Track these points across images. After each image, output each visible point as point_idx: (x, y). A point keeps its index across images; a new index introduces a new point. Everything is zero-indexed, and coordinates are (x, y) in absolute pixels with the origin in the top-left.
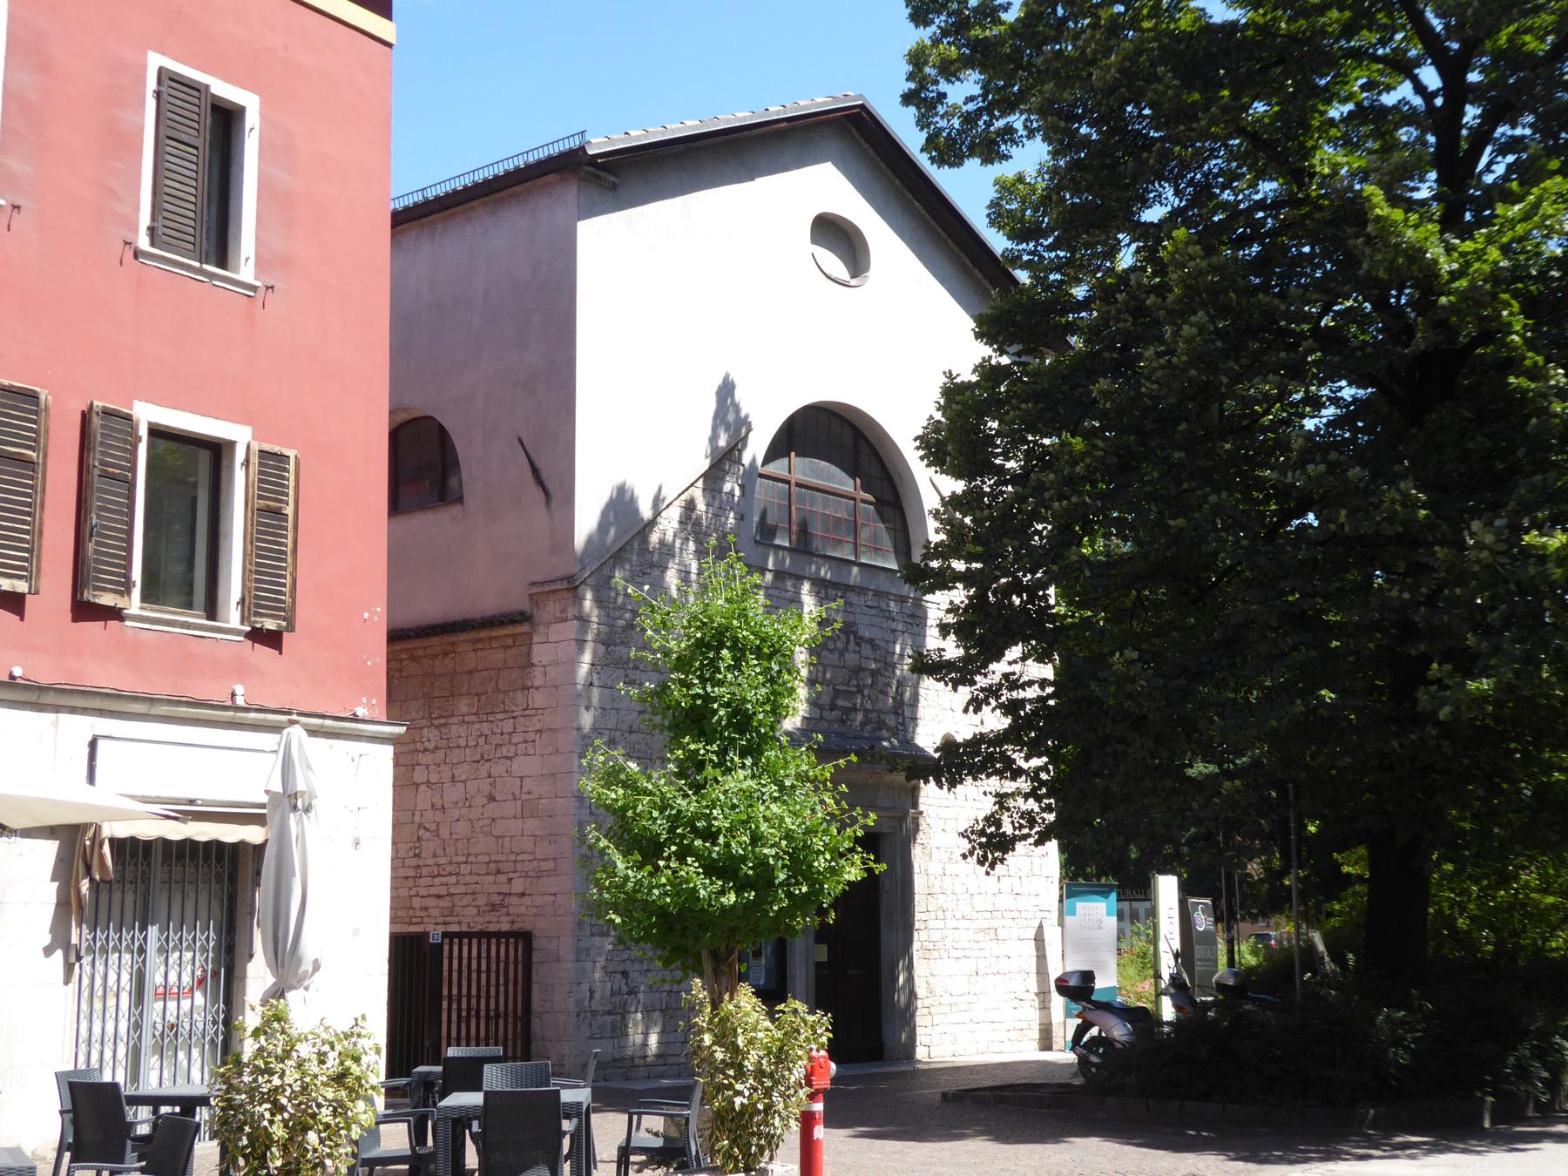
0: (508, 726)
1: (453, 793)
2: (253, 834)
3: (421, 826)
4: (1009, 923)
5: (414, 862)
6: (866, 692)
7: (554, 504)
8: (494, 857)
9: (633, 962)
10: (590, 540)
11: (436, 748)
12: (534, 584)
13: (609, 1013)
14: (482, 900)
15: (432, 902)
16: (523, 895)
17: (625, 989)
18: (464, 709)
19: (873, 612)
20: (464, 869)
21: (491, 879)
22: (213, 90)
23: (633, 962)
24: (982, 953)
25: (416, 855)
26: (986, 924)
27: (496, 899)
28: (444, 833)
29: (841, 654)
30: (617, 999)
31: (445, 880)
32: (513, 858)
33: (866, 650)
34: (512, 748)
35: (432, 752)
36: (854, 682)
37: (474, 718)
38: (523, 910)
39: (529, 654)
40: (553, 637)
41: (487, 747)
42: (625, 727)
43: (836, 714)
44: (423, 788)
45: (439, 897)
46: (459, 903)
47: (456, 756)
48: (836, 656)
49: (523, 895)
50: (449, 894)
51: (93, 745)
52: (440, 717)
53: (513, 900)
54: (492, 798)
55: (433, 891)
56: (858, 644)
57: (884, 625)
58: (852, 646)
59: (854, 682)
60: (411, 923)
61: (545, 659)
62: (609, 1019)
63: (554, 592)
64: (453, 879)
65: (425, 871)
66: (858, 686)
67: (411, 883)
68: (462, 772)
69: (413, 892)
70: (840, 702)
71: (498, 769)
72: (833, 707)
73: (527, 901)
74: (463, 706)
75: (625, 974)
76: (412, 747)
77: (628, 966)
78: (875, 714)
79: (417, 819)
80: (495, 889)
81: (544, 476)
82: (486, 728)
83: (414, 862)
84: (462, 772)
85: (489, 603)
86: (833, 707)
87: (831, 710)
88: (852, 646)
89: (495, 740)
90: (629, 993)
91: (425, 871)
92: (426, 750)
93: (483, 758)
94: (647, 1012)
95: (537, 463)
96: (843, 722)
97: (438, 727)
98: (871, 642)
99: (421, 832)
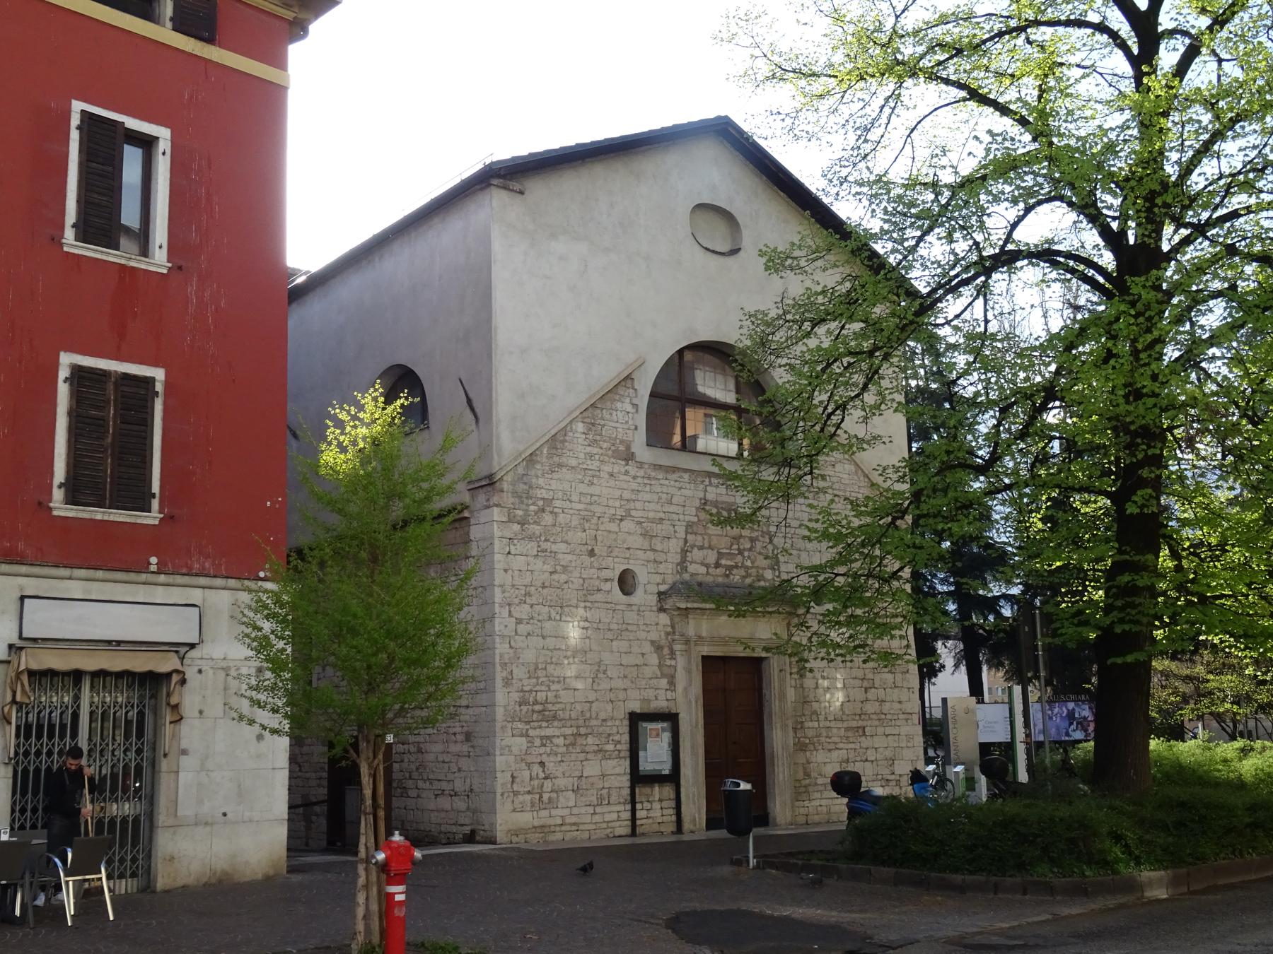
2: (165, 664)
6: (746, 554)
7: (481, 424)
13: (529, 792)
16: (468, 707)
22: (127, 125)
24: (852, 746)
26: (854, 724)
36: (735, 547)
39: (468, 534)
42: (539, 584)
43: (720, 571)
49: (468, 707)
51: (22, 598)
59: (735, 547)
61: (478, 536)
62: (528, 797)
63: (482, 487)
66: (739, 549)
72: (717, 565)
73: (470, 711)
75: (542, 764)
77: (544, 759)
81: (475, 405)
86: (717, 565)
94: (1045, 770)
95: (471, 395)
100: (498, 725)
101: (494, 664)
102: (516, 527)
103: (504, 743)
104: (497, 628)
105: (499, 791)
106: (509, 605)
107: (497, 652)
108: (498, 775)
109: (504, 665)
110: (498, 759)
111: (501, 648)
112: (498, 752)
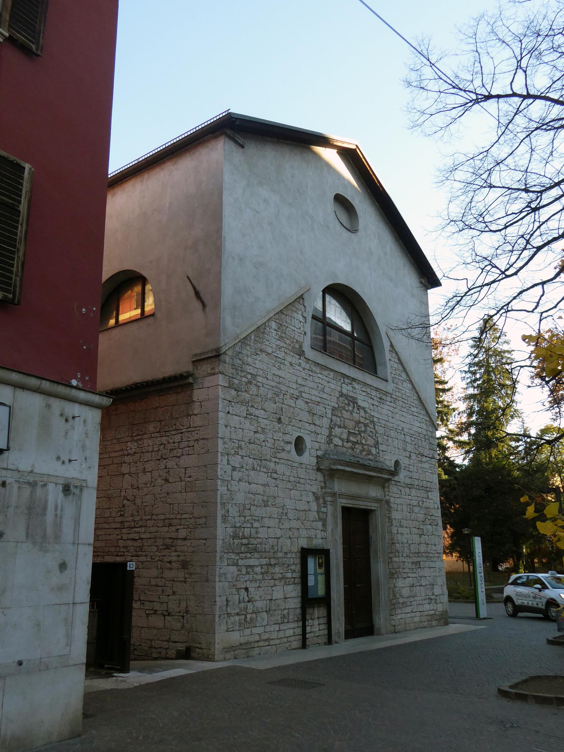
0: (177, 438)
1: (144, 478)
3: (125, 498)
4: (425, 559)
5: (121, 519)
6: (362, 435)
7: (207, 309)
8: (168, 516)
9: (251, 581)
10: (314, 150)
11: (135, 453)
12: (196, 355)
13: (238, 614)
14: (160, 542)
15: (130, 543)
16: (185, 539)
17: (246, 599)
18: (152, 430)
19: (364, 394)
20: (150, 523)
21: (166, 529)
23: (251, 581)
25: (121, 515)
27: (168, 542)
28: (138, 501)
29: (351, 414)
30: (242, 605)
31: (137, 530)
32: (179, 517)
33: (362, 413)
34: (180, 450)
35: (132, 455)
37: (158, 435)
38: (185, 548)
39: (191, 396)
40: (206, 384)
41: (165, 451)
43: (350, 444)
44: (127, 476)
45: (134, 540)
46: (145, 544)
47: (148, 456)
48: (349, 414)
49: (185, 539)
50: (142, 539)
52: (138, 435)
53: (179, 542)
54: (167, 480)
55: (131, 536)
56: (358, 409)
57: (369, 401)
58: (355, 410)
60: (117, 556)
62: (237, 618)
64: (143, 529)
65: (126, 524)
67: (118, 532)
68: (149, 467)
69: (119, 537)
70: (352, 439)
71: (171, 464)
73: (188, 543)
74: (151, 428)
76: (121, 453)
77: (248, 584)
78: (366, 447)
79: (123, 493)
80: (168, 535)
81: (202, 295)
82: (164, 440)
83: (121, 519)
84: (149, 467)
85: (169, 370)
87: (347, 442)
88: (355, 410)
89: (169, 447)
90: (249, 601)
91: (126, 524)
92: (128, 455)
93: (163, 458)
95: (198, 288)
96: (353, 449)
97: (136, 441)
98: (364, 408)
99: (125, 502)
100: (218, 555)
101: (216, 503)
102: (234, 393)
103: (222, 571)
104: (219, 473)
105: (217, 613)
106: (228, 454)
107: (219, 493)
108: (218, 599)
109: (223, 504)
110: (218, 585)
111: (222, 489)
112: (217, 579)
